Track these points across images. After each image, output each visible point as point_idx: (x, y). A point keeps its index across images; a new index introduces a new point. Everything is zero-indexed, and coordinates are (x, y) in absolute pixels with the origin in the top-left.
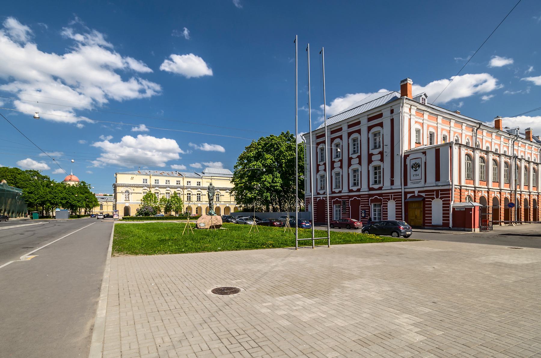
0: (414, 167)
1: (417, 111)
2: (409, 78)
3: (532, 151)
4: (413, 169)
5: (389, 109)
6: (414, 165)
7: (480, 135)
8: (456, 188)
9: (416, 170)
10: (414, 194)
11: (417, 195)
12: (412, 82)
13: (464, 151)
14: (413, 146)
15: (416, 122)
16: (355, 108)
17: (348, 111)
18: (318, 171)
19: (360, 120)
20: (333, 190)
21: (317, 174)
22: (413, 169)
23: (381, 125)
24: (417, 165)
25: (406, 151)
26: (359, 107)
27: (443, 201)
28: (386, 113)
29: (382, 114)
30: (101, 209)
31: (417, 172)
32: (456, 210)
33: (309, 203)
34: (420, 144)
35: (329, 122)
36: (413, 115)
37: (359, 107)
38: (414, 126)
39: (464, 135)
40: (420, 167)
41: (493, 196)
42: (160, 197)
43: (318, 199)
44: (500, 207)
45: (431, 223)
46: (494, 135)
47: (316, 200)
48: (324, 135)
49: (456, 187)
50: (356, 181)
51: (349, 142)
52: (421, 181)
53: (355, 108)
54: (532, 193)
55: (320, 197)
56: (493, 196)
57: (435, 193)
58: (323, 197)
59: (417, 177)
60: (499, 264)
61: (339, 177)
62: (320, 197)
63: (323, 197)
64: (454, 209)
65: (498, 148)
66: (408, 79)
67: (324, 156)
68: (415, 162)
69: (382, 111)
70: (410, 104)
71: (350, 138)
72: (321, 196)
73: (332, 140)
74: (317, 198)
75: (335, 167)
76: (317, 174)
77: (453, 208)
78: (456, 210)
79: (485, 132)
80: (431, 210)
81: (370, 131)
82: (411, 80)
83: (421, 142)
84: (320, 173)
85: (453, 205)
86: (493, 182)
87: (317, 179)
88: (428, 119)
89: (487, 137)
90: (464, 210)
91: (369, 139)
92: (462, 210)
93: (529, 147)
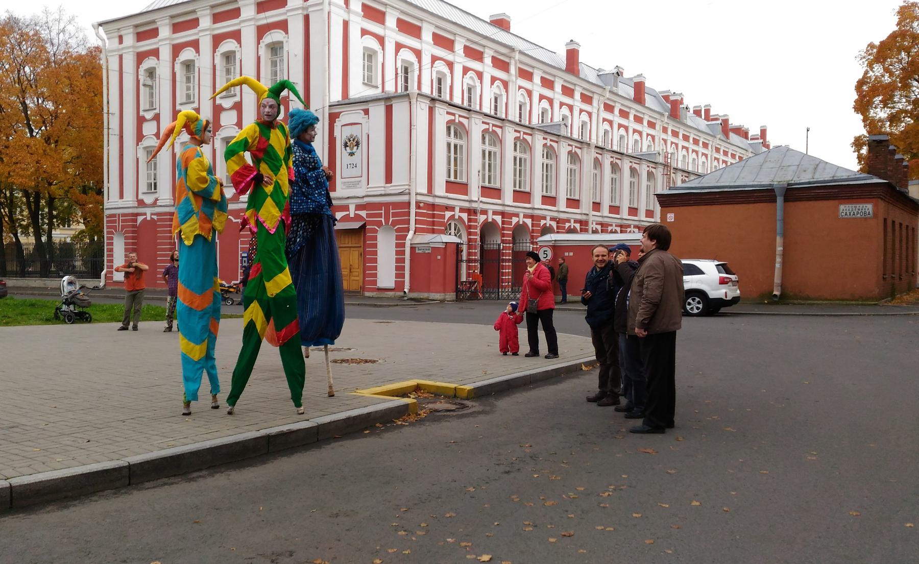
0: (348, 146)
1: (110, 35)
6: (350, 141)
9: (352, 154)
11: (353, 216)
15: (364, 32)
18: (140, 137)
20: (141, 197)
21: (138, 145)
23: (283, 25)
24: (354, 140)
27: (397, 231)
30: (536, 258)
31: (354, 159)
32: (417, 251)
33: (116, 231)
38: (358, 44)
40: (360, 147)
42: (223, 172)
43: (140, 219)
45: (375, 282)
47: (136, 221)
48: (154, 33)
49: (420, 198)
51: (175, 70)
52: (360, 181)
55: (145, 214)
57: (383, 212)
58: (152, 214)
59: (355, 172)
62: (145, 214)
63: (152, 214)
64: (413, 249)
67: (194, 95)
68: (350, 134)
71: (262, 45)
72: (148, 211)
73: (177, 50)
74: (137, 215)
75: (144, 134)
76: (138, 145)
77: (411, 248)
78: (417, 251)
84: (146, 143)
85: (411, 240)
87: (138, 160)
90: (430, 251)
91: (259, 58)
92: (427, 252)
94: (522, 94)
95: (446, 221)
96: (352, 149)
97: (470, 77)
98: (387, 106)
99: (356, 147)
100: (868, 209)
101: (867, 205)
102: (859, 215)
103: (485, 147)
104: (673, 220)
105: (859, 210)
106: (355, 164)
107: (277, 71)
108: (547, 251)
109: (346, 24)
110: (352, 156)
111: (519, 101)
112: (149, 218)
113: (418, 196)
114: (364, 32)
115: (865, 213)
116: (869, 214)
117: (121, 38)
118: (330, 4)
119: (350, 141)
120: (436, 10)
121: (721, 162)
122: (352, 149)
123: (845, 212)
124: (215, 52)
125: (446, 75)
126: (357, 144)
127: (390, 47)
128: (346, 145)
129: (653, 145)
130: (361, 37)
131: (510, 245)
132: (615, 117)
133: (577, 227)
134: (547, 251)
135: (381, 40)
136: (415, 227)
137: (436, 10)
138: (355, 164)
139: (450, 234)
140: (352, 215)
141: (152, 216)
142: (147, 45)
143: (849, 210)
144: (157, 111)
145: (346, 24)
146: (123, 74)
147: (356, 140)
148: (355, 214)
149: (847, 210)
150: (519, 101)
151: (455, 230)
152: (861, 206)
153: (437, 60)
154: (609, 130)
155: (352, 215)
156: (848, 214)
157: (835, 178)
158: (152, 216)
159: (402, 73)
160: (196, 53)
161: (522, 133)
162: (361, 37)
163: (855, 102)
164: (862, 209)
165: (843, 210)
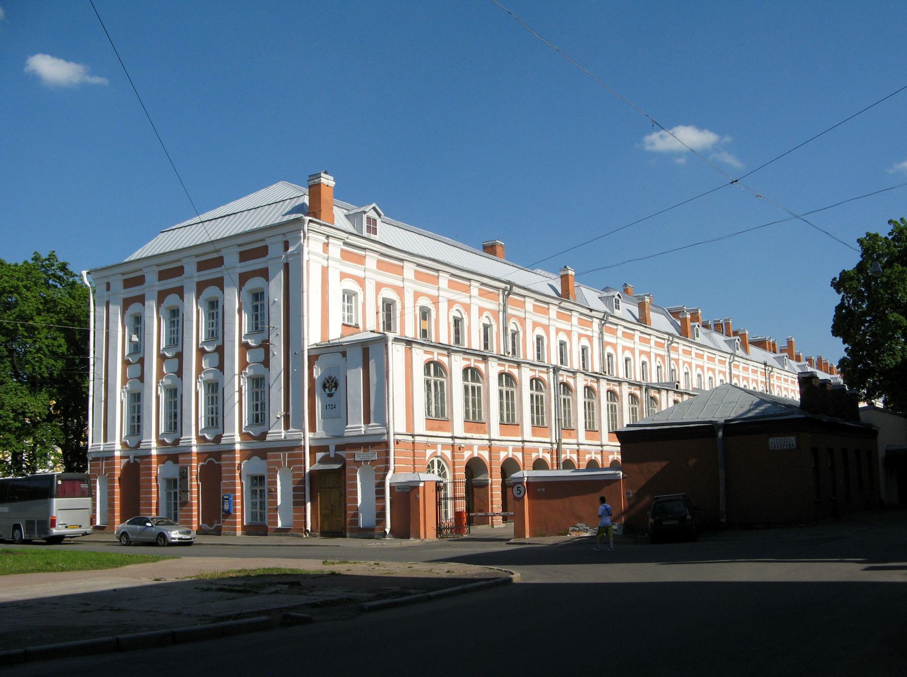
2: (326, 173)
3: (650, 347)
4: (325, 391)
5: (281, 239)
6: (328, 382)
7: (518, 310)
8: (397, 442)
9: (330, 395)
10: (336, 452)
12: (334, 183)
13: (420, 356)
14: (335, 334)
15: (343, 276)
16: (225, 216)
17: (215, 219)
19: (223, 253)
22: (325, 391)
24: (332, 382)
25: (315, 346)
26: (232, 214)
28: (275, 249)
29: (266, 247)
34: (358, 328)
35: (230, 228)
36: (335, 259)
37: (232, 214)
38: (336, 289)
39: (474, 311)
41: (533, 457)
44: (490, 481)
46: (553, 311)
49: (398, 437)
50: (259, 412)
53: (225, 216)
54: (605, 448)
56: (533, 457)
58: (135, 457)
60: (205, 586)
61: (261, 392)
63: (135, 457)
64: (391, 488)
65: (565, 341)
66: (323, 175)
68: (329, 375)
69: (268, 242)
70: (324, 234)
78: (396, 490)
79: (529, 304)
80: (376, 494)
81: (244, 286)
82: (332, 178)
83: (361, 325)
86: (500, 424)
88: (377, 270)
89: (535, 315)
93: (641, 339)
94: (514, 323)
95: (427, 458)
96: (330, 390)
97: (457, 310)
98: (363, 349)
99: (334, 389)
100: (792, 441)
101: (791, 438)
102: (785, 447)
103: (468, 383)
104: (17, 530)
105: (784, 442)
106: (333, 405)
107: (258, 315)
108: (520, 488)
109: (325, 271)
110: (330, 397)
111: (512, 330)
112: (132, 461)
113: (396, 436)
114: (343, 276)
115: (790, 444)
116: (793, 445)
117: (108, 287)
118: (308, 253)
119: (328, 382)
120: (422, 250)
121: (750, 381)
122: (330, 390)
123: (773, 444)
124: (199, 298)
125: (430, 310)
126: (336, 386)
127: (370, 287)
128: (324, 387)
129: (662, 365)
130: (341, 281)
131: (154, 514)
132: (618, 340)
133: (598, 458)
134: (520, 488)
135: (361, 281)
136: (395, 467)
137: (422, 250)
138: (333, 405)
139: (433, 472)
140: (332, 455)
141: (136, 459)
142: (134, 291)
143: (777, 442)
144: (141, 355)
145: (325, 271)
146: (110, 314)
147: (335, 381)
148: (335, 454)
149: (775, 442)
150: (512, 330)
151: (439, 468)
152: (786, 438)
153: (422, 296)
154: (613, 353)
155: (332, 455)
156: (776, 446)
157: (765, 414)
158: (136, 459)
159: (383, 311)
160: (181, 299)
161: (507, 366)
162: (341, 281)
163: (832, 327)
164: (787, 442)
165: (772, 442)
